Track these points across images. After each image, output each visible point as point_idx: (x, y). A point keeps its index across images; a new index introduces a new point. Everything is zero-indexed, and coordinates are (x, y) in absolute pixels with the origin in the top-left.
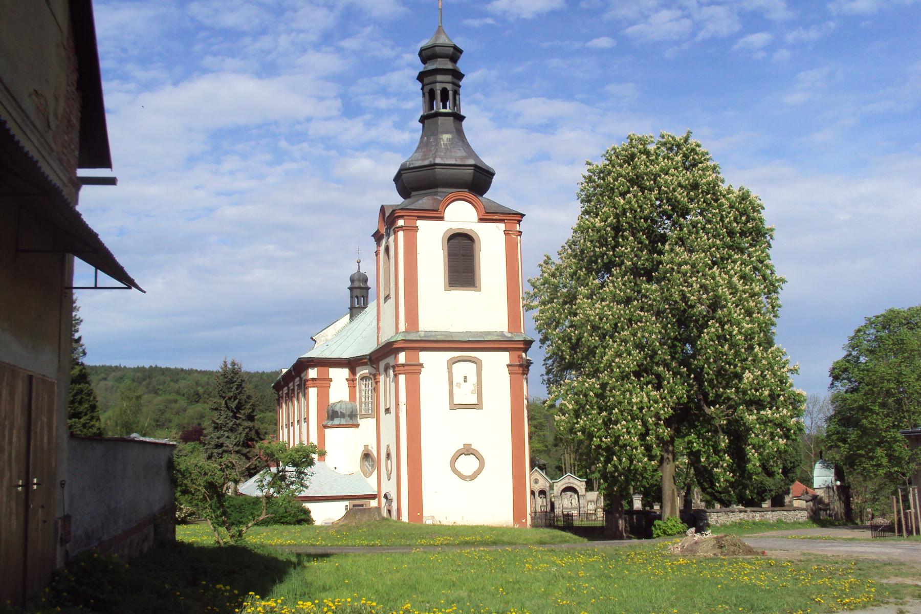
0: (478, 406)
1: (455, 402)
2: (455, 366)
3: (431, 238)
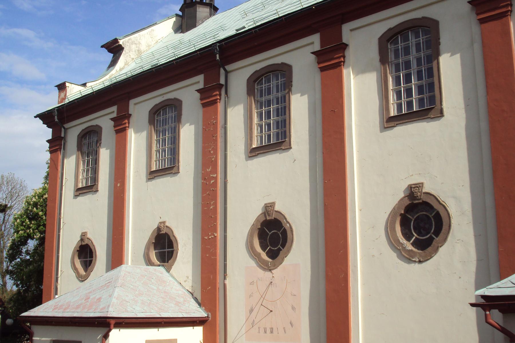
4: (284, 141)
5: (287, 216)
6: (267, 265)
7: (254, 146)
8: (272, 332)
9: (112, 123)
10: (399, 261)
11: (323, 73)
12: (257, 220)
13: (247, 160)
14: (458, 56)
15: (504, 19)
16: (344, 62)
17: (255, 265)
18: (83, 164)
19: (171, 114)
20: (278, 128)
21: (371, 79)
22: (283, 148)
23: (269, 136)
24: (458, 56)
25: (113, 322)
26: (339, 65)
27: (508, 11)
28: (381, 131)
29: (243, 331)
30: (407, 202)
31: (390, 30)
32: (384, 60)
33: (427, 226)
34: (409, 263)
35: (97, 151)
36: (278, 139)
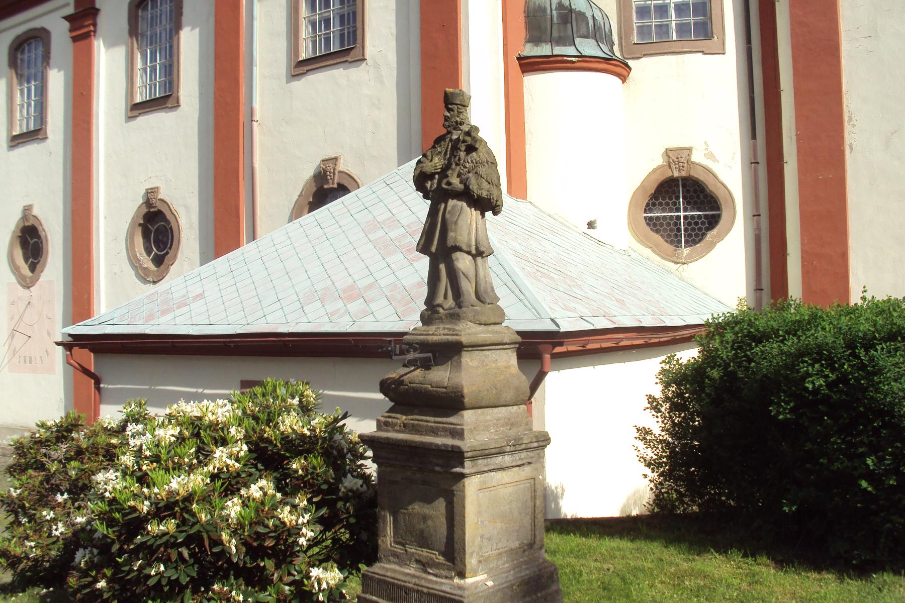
4: (170, 95)
5: (43, 222)
6: (25, 281)
7: (15, 133)
8: (30, 362)
9: (67, 25)
10: (137, 281)
11: (78, 44)
12: (17, 226)
13: (9, 150)
14: (197, 31)
15: (87, 41)
16: (95, 32)
17: (15, 281)
18: (142, 58)
19: (36, 51)
20: (342, 23)
21: (120, 52)
22: (350, 60)
23: (328, 40)
24: (197, 31)
26: (87, 36)
27: (89, 32)
28: (126, 122)
29: (6, 360)
30: (145, 210)
31: (18, 37)
32: (134, 31)
33: (165, 239)
34: (145, 283)
35: (43, 73)
36: (342, 44)
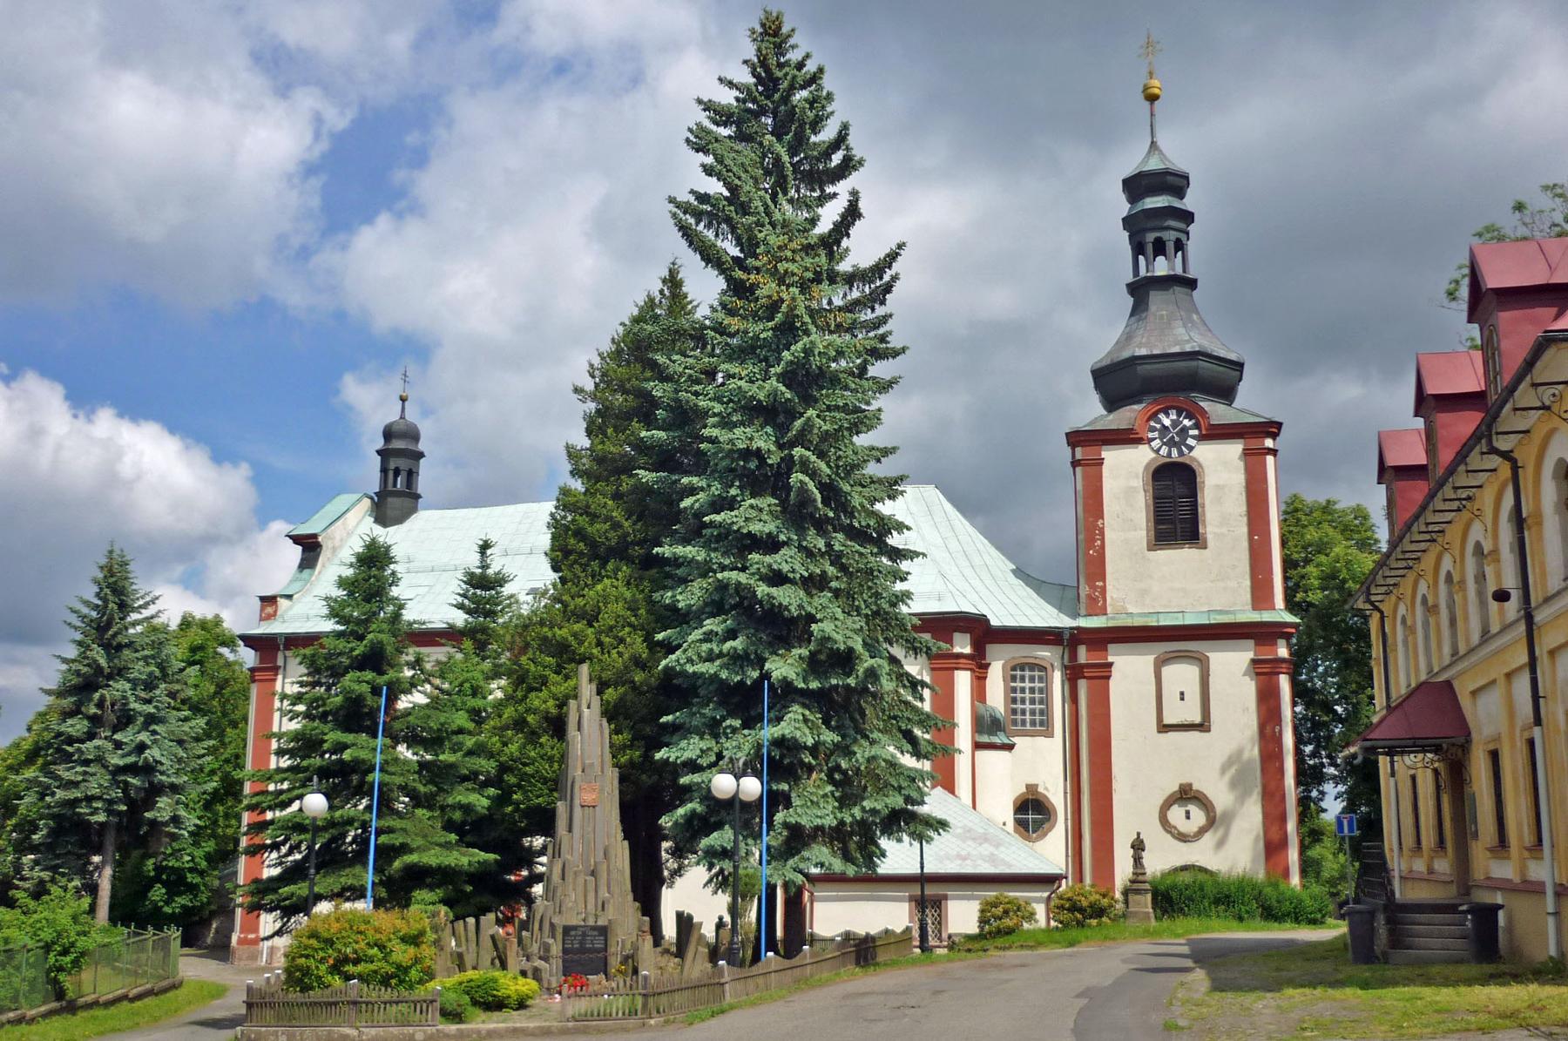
0: (1203, 726)
1: (1166, 721)
2: (1168, 671)
3: (1126, 472)
25: (281, 642)
